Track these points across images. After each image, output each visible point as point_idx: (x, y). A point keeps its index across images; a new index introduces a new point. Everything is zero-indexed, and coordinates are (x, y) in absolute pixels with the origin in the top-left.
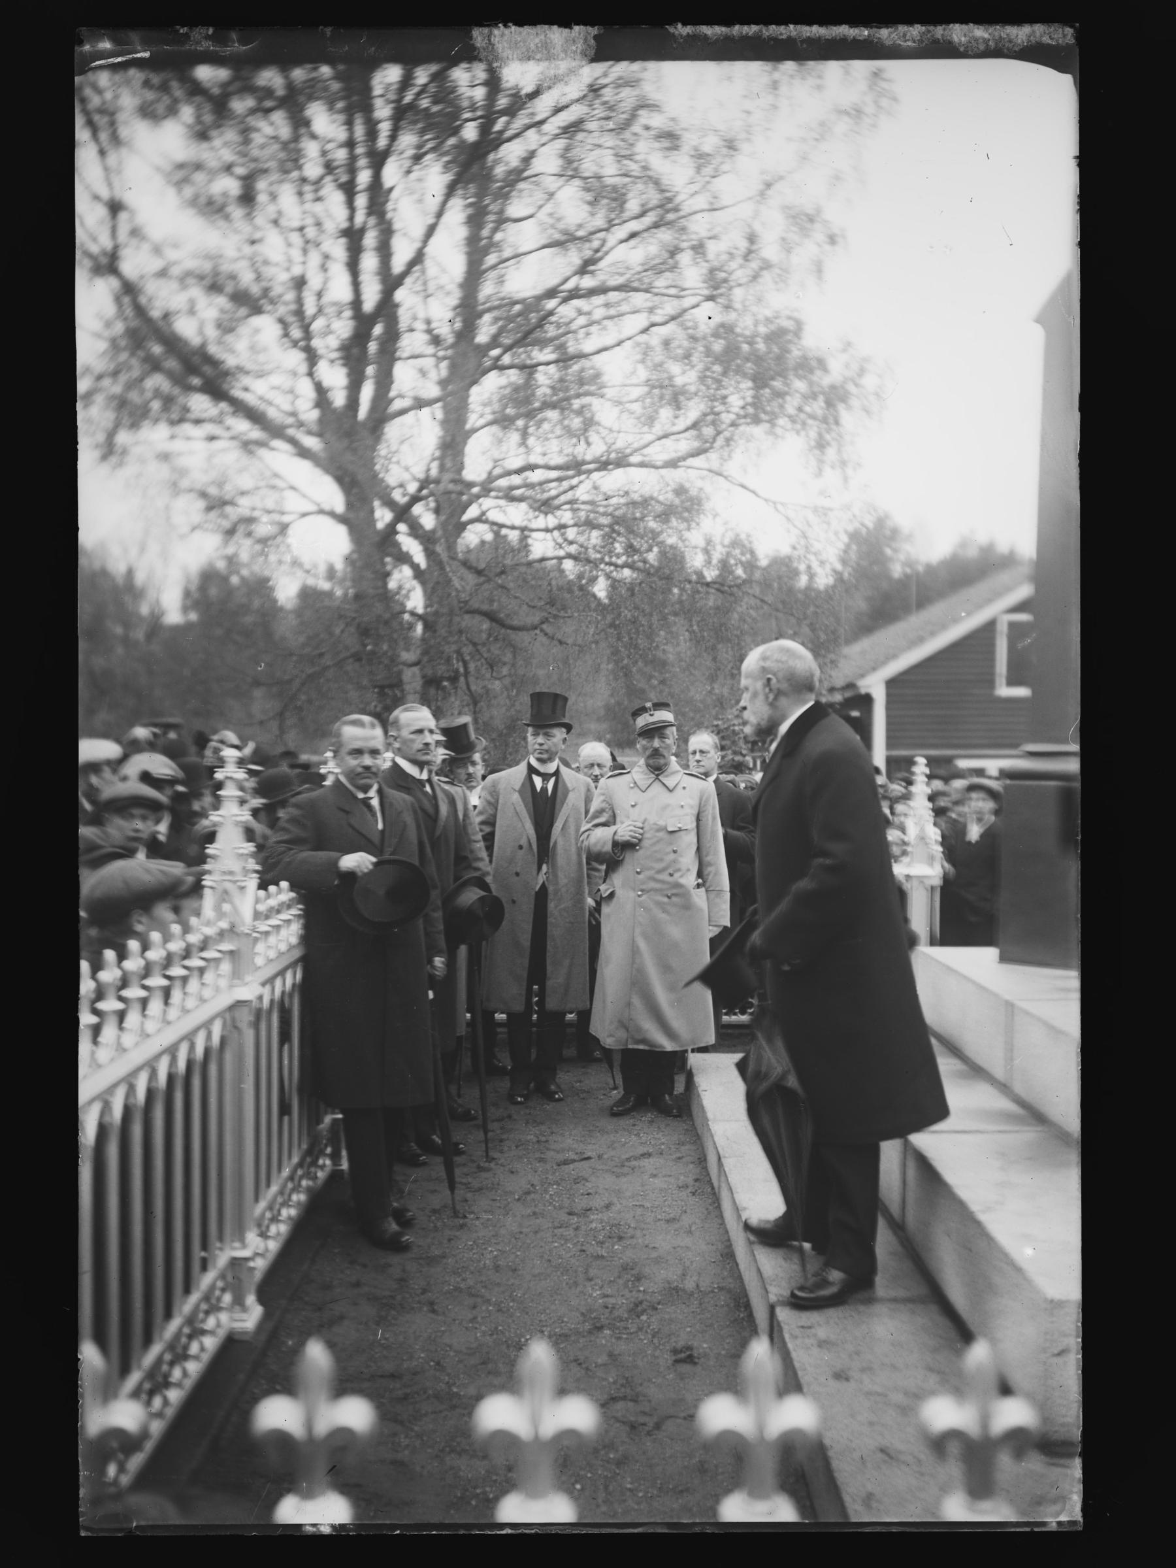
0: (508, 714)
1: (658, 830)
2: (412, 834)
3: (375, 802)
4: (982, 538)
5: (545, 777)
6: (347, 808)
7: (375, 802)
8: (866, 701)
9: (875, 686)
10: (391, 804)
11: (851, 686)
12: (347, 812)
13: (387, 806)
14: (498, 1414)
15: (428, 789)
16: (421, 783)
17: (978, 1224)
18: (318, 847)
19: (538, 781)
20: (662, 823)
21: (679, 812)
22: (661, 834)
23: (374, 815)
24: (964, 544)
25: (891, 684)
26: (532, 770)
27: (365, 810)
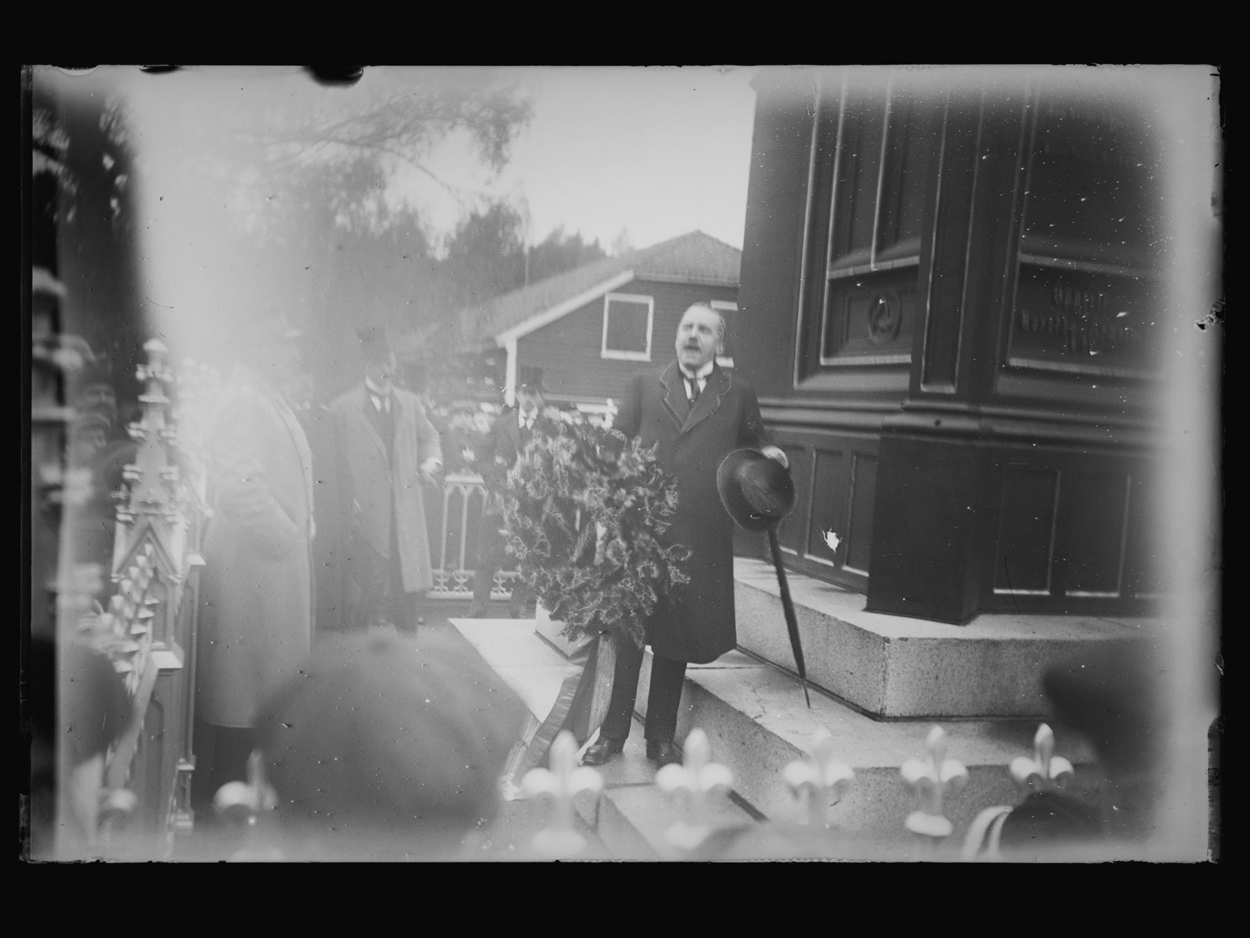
4: (570, 231)
5: (382, 398)
8: (503, 352)
9: (509, 341)
11: (491, 340)
19: (377, 402)
24: (556, 234)
25: (521, 341)
26: (370, 392)
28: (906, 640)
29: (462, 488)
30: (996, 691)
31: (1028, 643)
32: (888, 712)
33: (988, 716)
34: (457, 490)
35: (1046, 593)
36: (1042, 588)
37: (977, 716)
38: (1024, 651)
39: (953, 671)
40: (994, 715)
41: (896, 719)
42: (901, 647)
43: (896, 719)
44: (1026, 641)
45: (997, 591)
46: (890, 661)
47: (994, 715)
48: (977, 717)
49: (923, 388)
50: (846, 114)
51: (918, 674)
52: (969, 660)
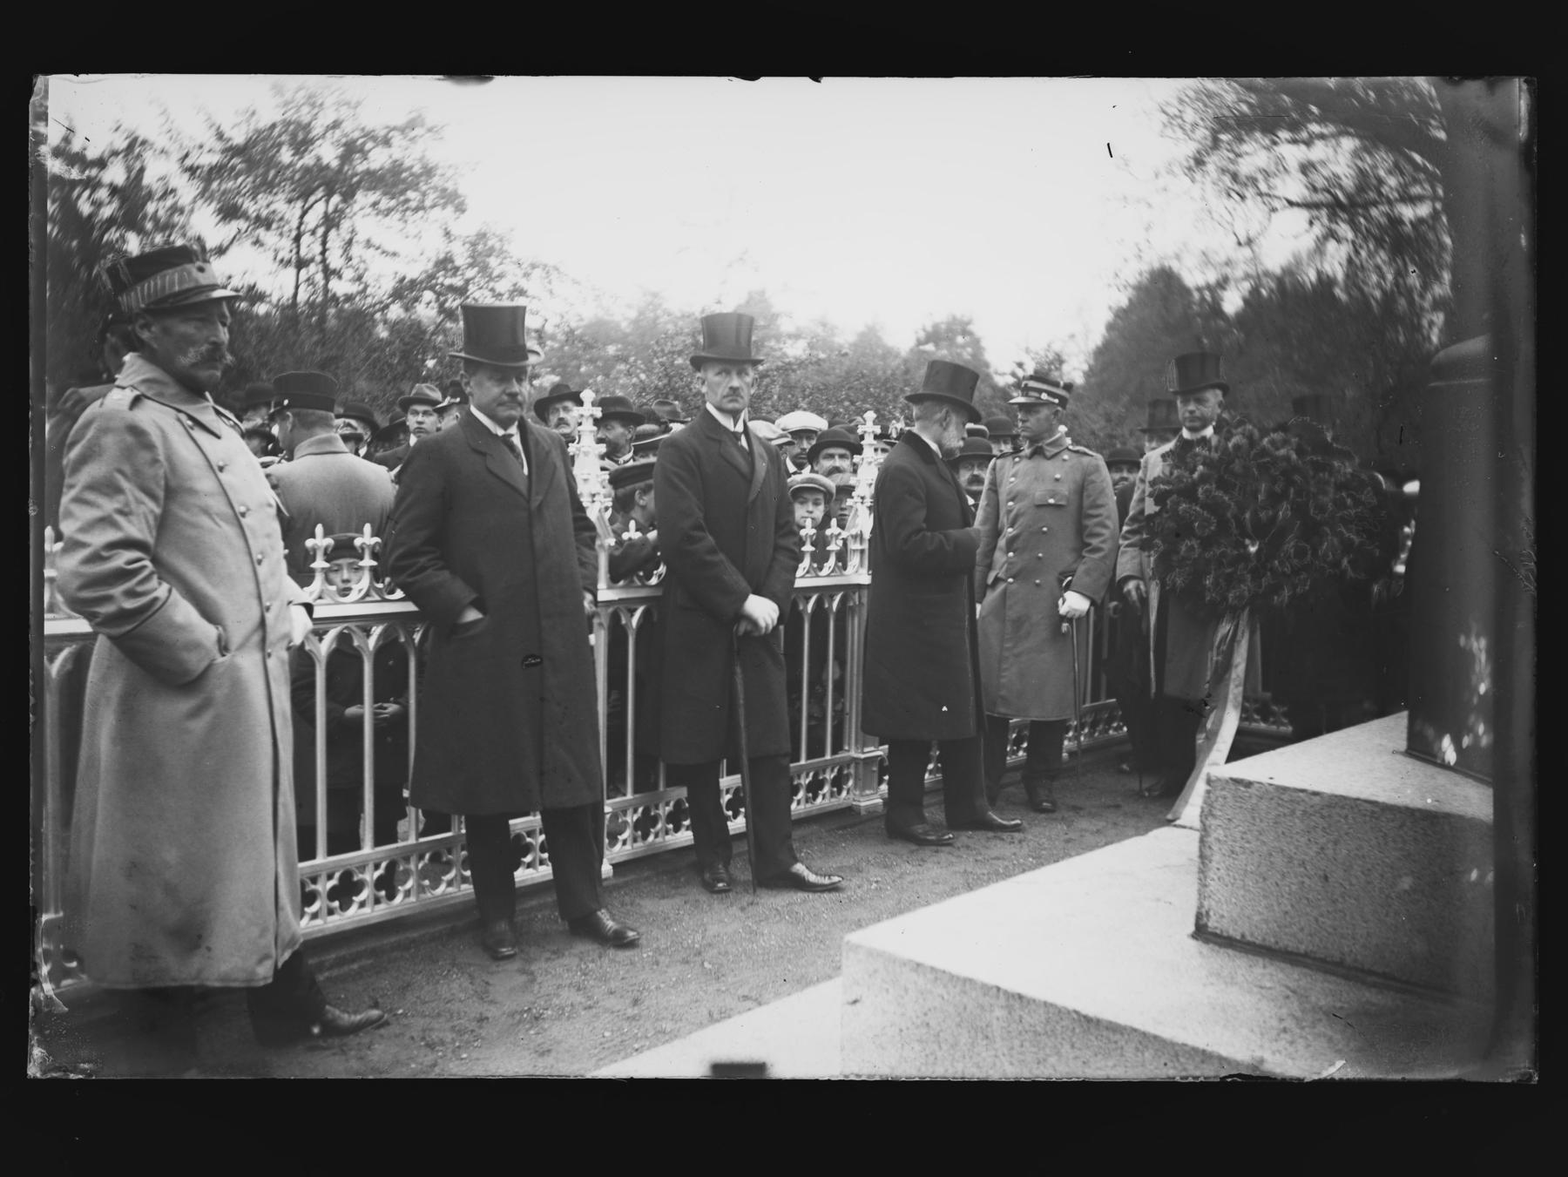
0: (270, 198)
2: (1370, 996)
3: (516, 440)
6: (483, 449)
7: (516, 440)
10: (537, 443)
12: (483, 454)
13: (532, 444)
14: (309, 543)
15: (744, 442)
16: (736, 436)
17: (1447, 816)
18: (751, 760)
23: (518, 456)
27: (507, 449)
51: (1279, 860)
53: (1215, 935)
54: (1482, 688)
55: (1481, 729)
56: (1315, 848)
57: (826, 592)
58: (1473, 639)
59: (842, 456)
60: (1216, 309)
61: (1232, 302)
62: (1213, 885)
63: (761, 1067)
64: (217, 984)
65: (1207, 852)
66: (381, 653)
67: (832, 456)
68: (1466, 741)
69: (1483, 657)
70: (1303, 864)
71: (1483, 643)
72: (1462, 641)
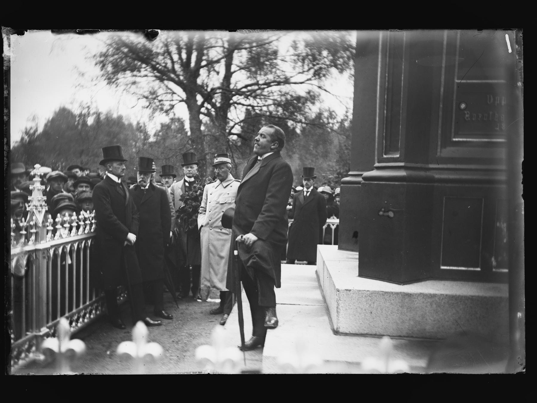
1: (217, 204)
20: (218, 200)
21: (227, 196)
22: (218, 205)
26: (185, 181)
28: (350, 290)
29: (332, 226)
30: (412, 323)
31: (434, 296)
32: (341, 330)
33: (407, 337)
34: (329, 226)
35: (479, 269)
36: (477, 267)
37: (400, 336)
38: (429, 300)
39: (381, 310)
40: (412, 337)
41: (346, 334)
42: (347, 294)
43: (346, 334)
44: (430, 294)
45: (442, 267)
46: (340, 302)
47: (412, 337)
48: (389, 336)
49: (385, 156)
50: (448, 37)
51: (359, 310)
52: (392, 304)
53: (342, 333)
54: (505, 241)
55: (505, 255)
56: (368, 305)
57: (57, 247)
58: (502, 223)
59: (86, 187)
60: (85, 123)
61: (90, 121)
62: (341, 319)
63: (258, 371)
64: (251, 341)
65: (339, 310)
66: (335, 229)
67: (82, 187)
68: (500, 259)
69: (505, 230)
70: (365, 310)
71: (505, 225)
72: (498, 224)
